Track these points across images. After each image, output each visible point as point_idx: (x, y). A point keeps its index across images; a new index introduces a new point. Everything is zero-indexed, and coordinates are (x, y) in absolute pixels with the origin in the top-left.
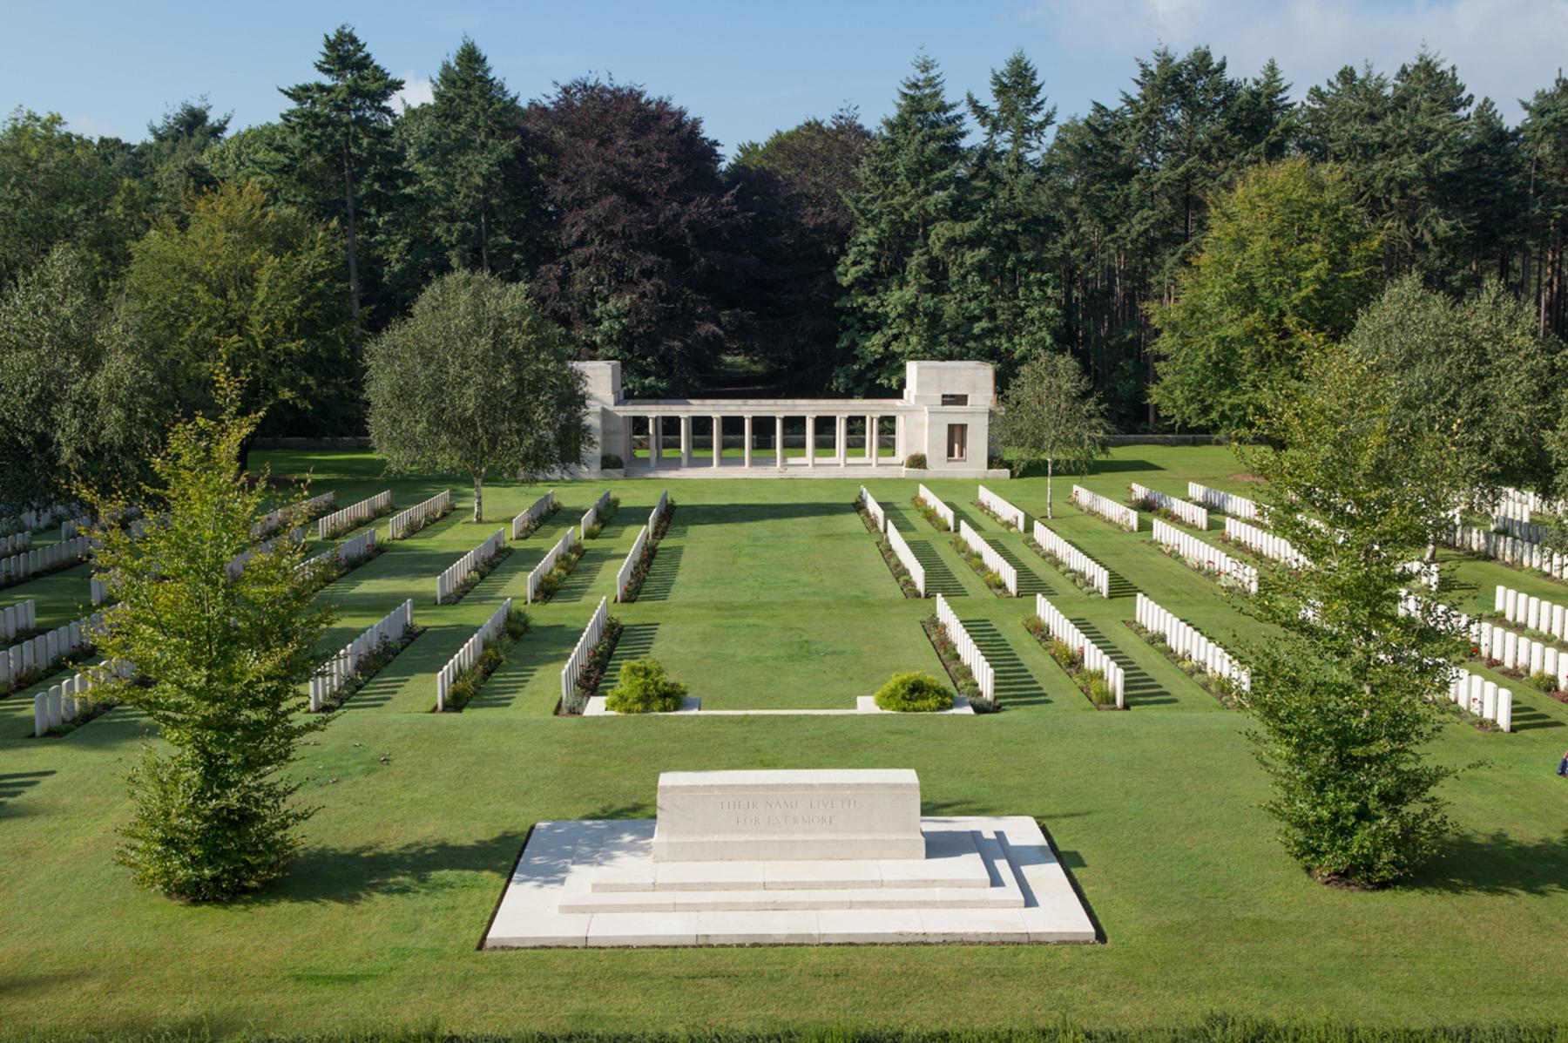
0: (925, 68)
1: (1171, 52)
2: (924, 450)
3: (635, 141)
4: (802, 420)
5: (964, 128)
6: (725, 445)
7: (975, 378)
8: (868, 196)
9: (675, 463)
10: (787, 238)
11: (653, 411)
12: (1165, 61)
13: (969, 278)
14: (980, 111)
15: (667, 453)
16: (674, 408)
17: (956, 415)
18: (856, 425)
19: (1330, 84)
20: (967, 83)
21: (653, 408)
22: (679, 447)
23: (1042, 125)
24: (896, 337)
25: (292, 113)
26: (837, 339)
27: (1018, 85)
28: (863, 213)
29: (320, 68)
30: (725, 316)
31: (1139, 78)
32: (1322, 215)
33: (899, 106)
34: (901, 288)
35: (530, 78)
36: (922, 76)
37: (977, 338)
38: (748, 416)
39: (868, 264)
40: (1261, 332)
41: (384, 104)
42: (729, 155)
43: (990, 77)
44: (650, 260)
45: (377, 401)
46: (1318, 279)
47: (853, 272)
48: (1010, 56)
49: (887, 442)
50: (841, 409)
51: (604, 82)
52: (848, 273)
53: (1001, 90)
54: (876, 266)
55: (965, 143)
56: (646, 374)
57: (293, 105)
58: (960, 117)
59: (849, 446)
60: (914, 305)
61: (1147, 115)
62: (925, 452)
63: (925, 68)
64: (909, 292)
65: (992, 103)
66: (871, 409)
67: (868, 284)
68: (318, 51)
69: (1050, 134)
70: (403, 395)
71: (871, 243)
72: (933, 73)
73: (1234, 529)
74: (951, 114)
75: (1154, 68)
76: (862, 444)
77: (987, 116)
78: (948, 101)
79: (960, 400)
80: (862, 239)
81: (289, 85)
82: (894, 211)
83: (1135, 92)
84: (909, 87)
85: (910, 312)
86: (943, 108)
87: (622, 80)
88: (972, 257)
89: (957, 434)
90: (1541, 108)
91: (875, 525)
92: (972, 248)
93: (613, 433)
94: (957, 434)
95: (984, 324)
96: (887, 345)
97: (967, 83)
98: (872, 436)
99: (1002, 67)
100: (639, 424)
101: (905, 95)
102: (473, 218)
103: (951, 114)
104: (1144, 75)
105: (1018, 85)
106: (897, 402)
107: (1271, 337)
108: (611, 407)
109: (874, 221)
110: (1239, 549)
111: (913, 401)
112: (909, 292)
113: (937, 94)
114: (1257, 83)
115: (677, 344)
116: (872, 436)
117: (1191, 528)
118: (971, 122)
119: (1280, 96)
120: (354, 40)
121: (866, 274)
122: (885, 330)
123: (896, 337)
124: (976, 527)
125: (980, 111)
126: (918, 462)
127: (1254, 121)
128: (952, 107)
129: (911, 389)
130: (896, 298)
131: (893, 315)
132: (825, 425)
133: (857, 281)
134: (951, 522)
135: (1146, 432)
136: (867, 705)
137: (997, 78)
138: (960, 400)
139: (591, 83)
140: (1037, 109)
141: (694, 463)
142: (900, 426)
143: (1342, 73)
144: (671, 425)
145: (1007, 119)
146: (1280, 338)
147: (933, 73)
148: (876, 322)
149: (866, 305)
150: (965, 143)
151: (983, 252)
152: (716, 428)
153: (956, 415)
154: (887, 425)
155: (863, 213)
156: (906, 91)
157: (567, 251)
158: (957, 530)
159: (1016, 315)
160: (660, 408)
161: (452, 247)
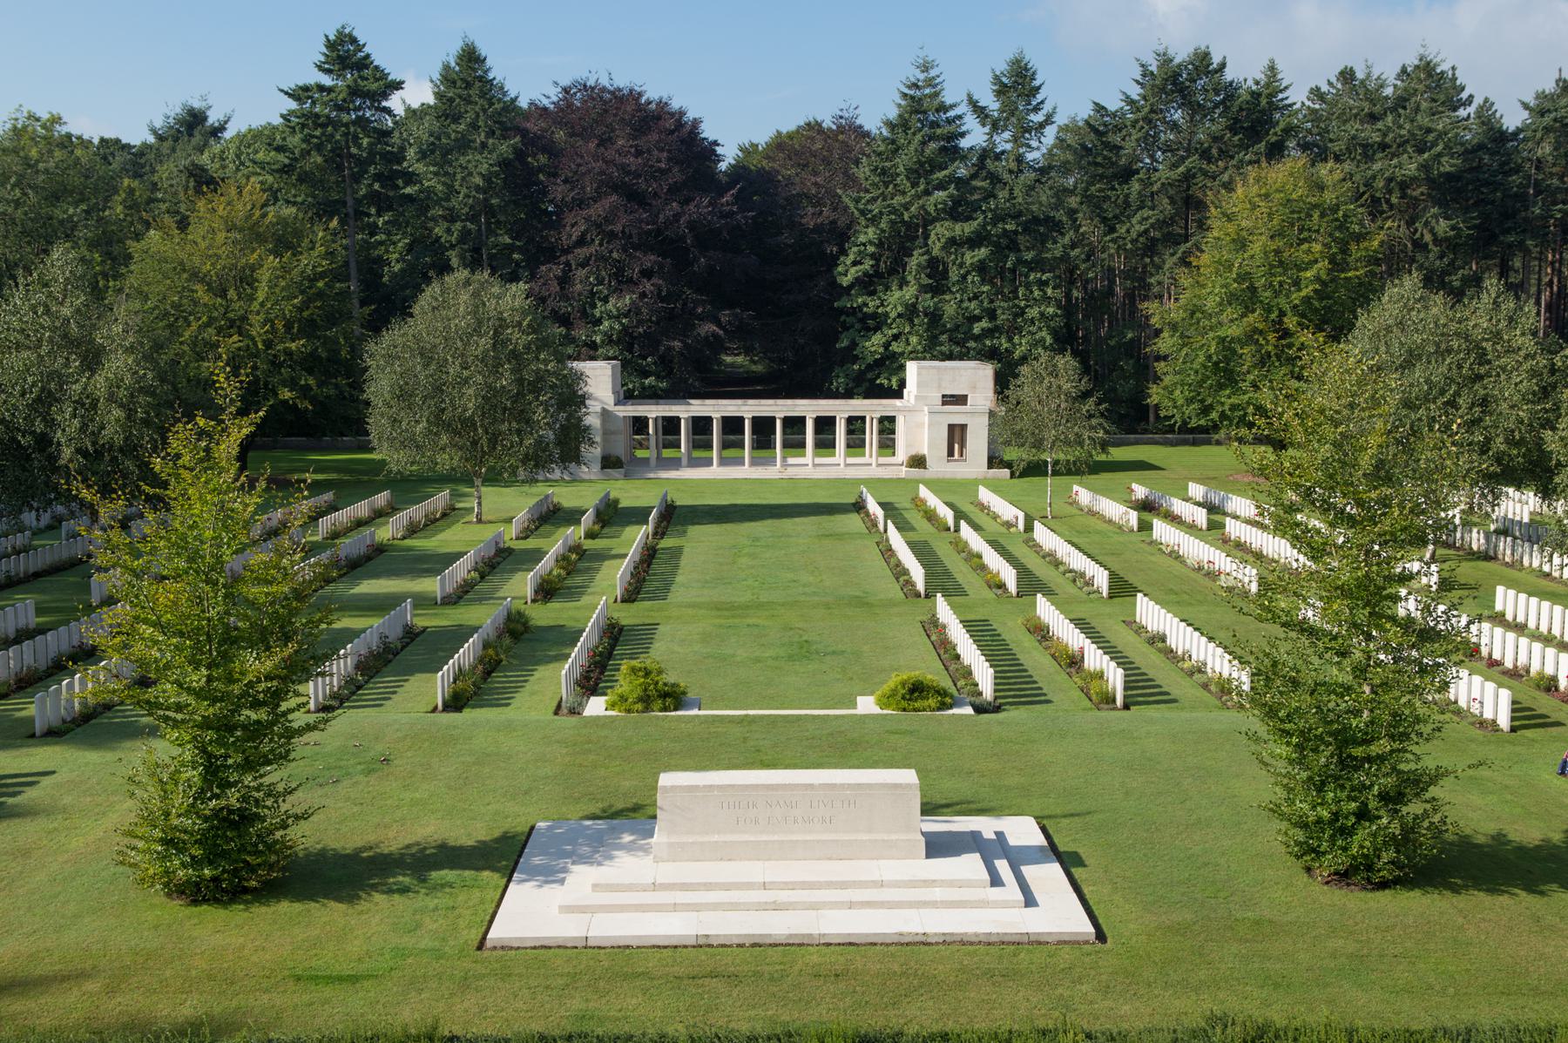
0: (925, 68)
1: (1171, 52)
2: (924, 450)
3: (635, 141)
4: (802, 420)
5: (964, 128)
6: (725, 445)
7: (975, 378)
8: (868, 196)
9: (675, 463)
10: (787, 238)
11: (653, 411)
12: (1165, 60)
13: (970, 278)
14: (980, 111)
15: (667, 453)
16: (674, 408)
17: (956, 415)
18: (856, 425)
19: (1330, 83)
20: (967, 83)
21: (653, 408)
22: (679, 447)
23: (1042, 125)
24: (896, 337)
25: (291, 113)
26: (837, 340)
27: (1018, 85)
28: (863, 213)
29: (320, 68)
30: (725, 316)
31: (1139, 78)
32: (1322, 215)
33: (899, 106)
34: (901, 288)
35: (530, 78)
36: (922, 76)
37: (977, 338)
38: (748, 416)
39: (868, 264)
40: (1261, 332)
41: (384, 104)
42: (729, 155)
43: (990, 77)
44: (650, 260)
45: (377, 401)
46: (1318, 279)
47: (853, 272)
48: (1010, 56)
49: (887, 441)
50: (841, 409)
51: (604, 82)
52: (848, 273)
53: (1001, 90)
54: (876, 266)
55: (965, 143)
56: (646, 374)
57: (293, 105)
58: (960, 117)
59: (849, 446)
60: (914, 305)
61: (1147, 115)
62: (925, 452)
63: (925, 68)
64: (909, 292)
65: (991, 103)
66: (871, 409)
67: (868, 284)
68: (318, 51)
69: (1050, 134)
70: (403, 395)
71: (871, 243)
72: (933, 73)
73: (1234, 529)
74: (951, 114)
75: (1154, 68)
76: (862, 444)
77: (987, 116)
78: (948, 101)
79: (960, 400)
80: (862, 239)
81: (289, 85)
82: (894, 211)
83: (1135, 92)
84: (909, 87)
85: (910, 312)
86: (943, 108)
87: (623, 81)
88: (971, 257)
89: (957, 434)
90: (1541, 108)
91: (875, 525)
92: (972, 248)
93: (613, 433)
94: (957, 434)
95: (984, 324)
96: (887, 346)
97: (967, 83)
98: (872, 436)
99: (1002, 67)
100: (639, 424)
101: (905, 95)
102: (473, 218)
103: (951, 114)
104: (1144, 76)
105: (1018, 85)
106: (897, 402)
107: (1271, 337)
108: (611, 407)
109: (874, 221)
110: (1239, 549)
111: (912, 401)
112: (909, 292)
113: (936, 94)
114: (1257, 83)
115: (677, 344)
116: (872, 436)
117: (1191, 528)
118: (971, 122)
119: (1281, 96)
120: (354, 40)
121: (866, 274)
122: (885, 330)
123: (896, 337)
124: (976, 527)
125: (980, 111)
126: (918, 462)
127: (1254, 121)
128: (952, 106)
129: (911, 390)
130: (896, 299)
131: (893, 315)
132: (825, 425)
133: (857, 281)
134: (951, 522)
135: (1145, 431)
136: (867, 705)
137: (996, 78)
138: (960, 400)
139: (591, 83)
140: (1036, 109)
141: (694, 463)
142: (900, 426)
143: (1342, 73)
144: (671, 425)
145: (1007, 119)
146: (1280, 338)
147: (933, 73)
148: (875, 322)
149: (866, 305)
150: (965, 143)
151: (983, 252)
152: (716, 428)
153: (956, 415)
154: (887, 425)
155: (863, 213)
156: (906, 91)
157: (567, 251)
158: (957, 530)
159: (1016, 315)
160: (660, 408)
161: (453, 247)
